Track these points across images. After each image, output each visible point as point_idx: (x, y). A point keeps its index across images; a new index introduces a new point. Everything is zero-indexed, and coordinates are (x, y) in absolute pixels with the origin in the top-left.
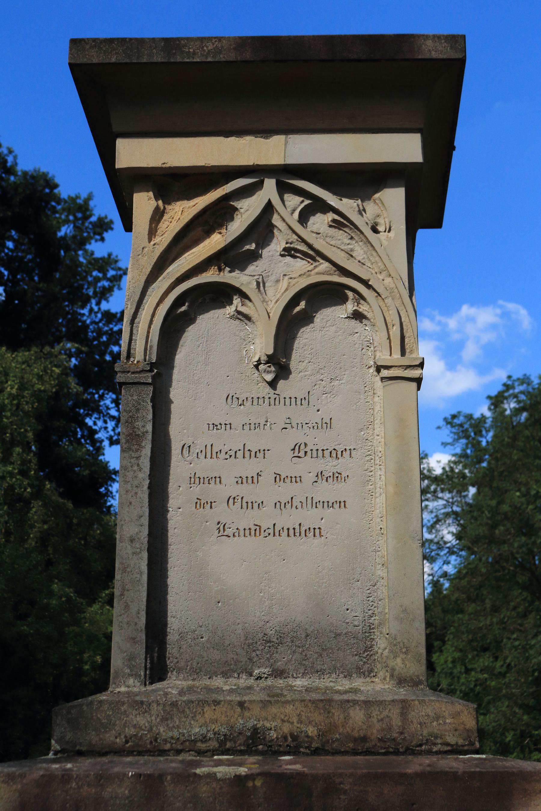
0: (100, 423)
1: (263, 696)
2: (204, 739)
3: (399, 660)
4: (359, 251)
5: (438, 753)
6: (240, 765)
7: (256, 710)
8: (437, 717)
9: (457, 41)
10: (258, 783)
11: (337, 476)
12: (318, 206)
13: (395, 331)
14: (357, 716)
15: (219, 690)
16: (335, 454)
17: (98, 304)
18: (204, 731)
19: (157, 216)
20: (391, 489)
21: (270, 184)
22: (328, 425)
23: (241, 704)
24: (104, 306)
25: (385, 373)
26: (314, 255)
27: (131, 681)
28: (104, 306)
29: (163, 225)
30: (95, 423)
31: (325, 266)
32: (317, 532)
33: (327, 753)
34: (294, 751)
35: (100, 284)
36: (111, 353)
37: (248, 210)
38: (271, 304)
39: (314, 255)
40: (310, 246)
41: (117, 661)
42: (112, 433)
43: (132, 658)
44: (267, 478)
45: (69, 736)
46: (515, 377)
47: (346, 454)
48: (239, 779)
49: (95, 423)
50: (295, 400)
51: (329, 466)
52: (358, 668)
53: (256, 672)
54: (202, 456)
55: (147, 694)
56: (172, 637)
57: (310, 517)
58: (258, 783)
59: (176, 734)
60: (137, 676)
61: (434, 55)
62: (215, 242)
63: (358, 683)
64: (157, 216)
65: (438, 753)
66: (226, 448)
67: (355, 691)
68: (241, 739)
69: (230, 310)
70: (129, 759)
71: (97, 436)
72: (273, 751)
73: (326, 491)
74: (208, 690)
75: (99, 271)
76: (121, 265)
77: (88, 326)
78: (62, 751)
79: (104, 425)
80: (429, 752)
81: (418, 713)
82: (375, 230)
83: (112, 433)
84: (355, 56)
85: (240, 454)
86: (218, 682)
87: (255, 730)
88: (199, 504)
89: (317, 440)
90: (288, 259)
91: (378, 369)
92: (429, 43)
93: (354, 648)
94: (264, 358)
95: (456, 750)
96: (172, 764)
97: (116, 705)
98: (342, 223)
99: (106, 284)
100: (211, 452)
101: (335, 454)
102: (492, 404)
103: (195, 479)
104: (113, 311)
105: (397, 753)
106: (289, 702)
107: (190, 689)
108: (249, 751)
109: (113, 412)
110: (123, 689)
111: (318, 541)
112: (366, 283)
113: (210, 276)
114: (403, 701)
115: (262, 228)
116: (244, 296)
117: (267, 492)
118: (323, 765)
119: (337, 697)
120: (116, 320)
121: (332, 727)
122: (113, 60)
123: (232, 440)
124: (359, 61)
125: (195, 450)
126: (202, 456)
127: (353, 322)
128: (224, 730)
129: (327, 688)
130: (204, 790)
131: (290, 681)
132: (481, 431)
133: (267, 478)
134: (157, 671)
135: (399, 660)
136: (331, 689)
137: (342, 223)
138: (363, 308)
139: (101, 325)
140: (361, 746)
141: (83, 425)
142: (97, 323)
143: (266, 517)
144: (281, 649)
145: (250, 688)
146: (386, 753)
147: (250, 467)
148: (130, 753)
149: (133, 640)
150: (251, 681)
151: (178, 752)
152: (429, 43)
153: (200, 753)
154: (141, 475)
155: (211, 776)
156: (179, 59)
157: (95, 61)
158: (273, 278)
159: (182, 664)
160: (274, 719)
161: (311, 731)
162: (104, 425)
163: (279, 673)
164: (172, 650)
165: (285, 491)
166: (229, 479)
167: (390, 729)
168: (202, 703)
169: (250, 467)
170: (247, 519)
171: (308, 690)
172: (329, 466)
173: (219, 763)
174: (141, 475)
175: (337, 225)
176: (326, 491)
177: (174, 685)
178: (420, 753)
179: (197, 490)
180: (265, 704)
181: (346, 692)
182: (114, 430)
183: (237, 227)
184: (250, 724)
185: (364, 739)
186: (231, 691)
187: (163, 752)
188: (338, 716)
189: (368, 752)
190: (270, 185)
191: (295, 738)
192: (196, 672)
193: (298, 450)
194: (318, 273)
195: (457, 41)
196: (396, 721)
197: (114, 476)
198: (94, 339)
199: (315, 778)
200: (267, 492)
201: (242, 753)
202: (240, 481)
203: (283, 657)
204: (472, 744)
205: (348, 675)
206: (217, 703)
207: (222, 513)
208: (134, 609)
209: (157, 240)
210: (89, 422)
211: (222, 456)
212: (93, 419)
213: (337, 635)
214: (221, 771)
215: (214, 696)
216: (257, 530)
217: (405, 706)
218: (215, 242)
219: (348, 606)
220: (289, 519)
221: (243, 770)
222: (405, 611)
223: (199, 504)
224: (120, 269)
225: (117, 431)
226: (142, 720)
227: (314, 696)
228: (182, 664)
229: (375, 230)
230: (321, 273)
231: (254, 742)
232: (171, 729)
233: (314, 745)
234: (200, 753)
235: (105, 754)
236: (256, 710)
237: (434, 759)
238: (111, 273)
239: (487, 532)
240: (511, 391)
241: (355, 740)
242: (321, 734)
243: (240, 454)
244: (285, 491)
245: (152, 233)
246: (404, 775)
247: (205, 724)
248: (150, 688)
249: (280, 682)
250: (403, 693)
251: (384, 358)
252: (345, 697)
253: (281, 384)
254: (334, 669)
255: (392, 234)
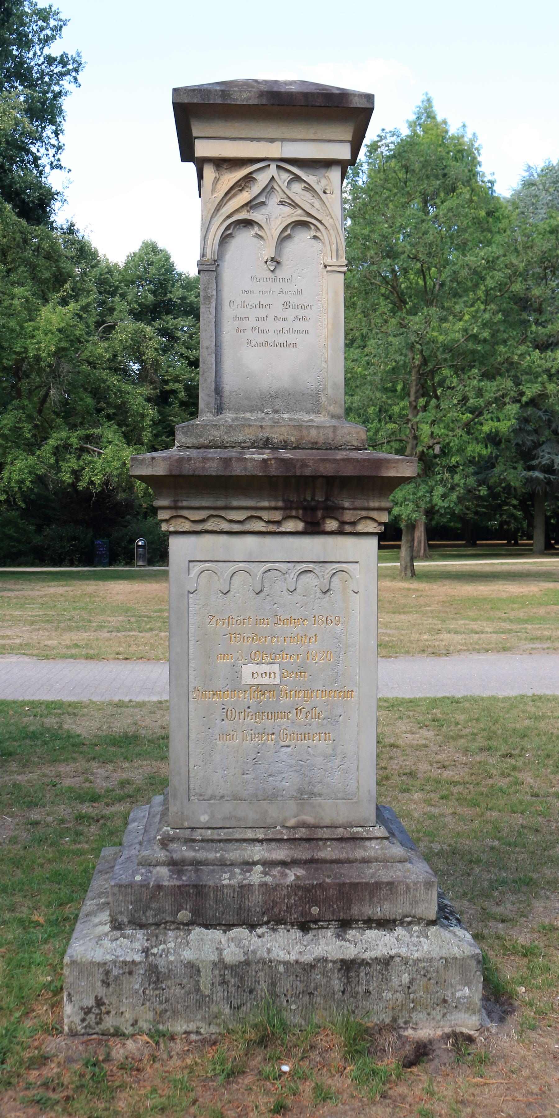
0: (43, 150)
1: (270, 423)
2: (245, 442)
3: (332, 407)
4: (317, 203)
5: (349, 449)
6: (263, 454)
7: (268, 429)
8: (349, 434)
9: (370, 98)
10: (273, 462)
11: (304, 318)
12: (297, 178)
13: (334, 247)
14: (314, 432)
15: (249, 419)
16: (303, 307)
17: (41, 49)
18: (244, 438)
19: (216, 180)
20: (330, 326)
21: (273, 166)
22: (300, 292)
23: (261, 426)
24: (47, 51)
25: (328, 268)
26: (295, 205)
27: (208, 414)
28: (47, 51)
29: (219, 186)
30: (38, 151)
31: (300, 211)
32: (295, 345)
33: (299, 448)
34: (285, 448)
35: (44, 33)
36: (53, 92)
37: (262, 179)
38: (273, 231)
39: (295, 205)
40: (293, 201)
41: (201, 405)
42: (52, 159)
43: (208, 404)
44: (271, 318)
45: (183, 440)
46: (387, 130)
47: (309, 308)
48: (264, 461)
49: (38, 151)
50: (284, 280)
51: (301, 313)
52: (313, 410)
53: (265, 411)
54: (239, 307)
55: (218, 421)
56: (226, 394)
57: (291, 338)
58: (273, 462)
59: (232, 439)
60: (211, 412)
61: (359, 106)
62: (245, 197)
63: (313, 417)
64: (216, 180)
65: (349, 449)
66: (250, 303)
67: (312, 421)
68: (261, 442)
69: (253, 233)
70: (212, 450)
71: (39, 162)
72: (276, 448)
73: (299, 325)
74: (246, 419)
75: (44, 22)
76: (61, 16)
77: (32, 68)
78: (180, 446)
79: (46, 152)
80: (345, 449)
81: (340, 432)
82: (325, 192)
83: (52, 159)
84: (318, 104)
85: (258, 306)
86: (248, 415)
87: (268, 439)
88: (238, 330)
89: (295, 300)
90: (281, 206)
91: (325, 266)
92: (356, 98)
93: (312, 401)
94: (269, 259)
95: (357, 449)
96: (233, 453)
97: (204, 426)
98: (309, 188)
99: (49, 32)
100: (244, 305)
101: (303, 307)
102: (368, 151)
103: (236, 318)
104: (53, 55)
105: (331, 449)
106: (283, 424)
107: (236, 418)
108: (265, 447)
109: (54, 141)
110: (205, 418)
111: (295, 349)
112: (320, 221)
113: (243, 215)
114: (334, 426)
115: (269, 189)
116: (260, 226)
117: (271, 325)
118: (299, 455)
119: (304, 424)
120: (56, 63)
121: (302, 438)
122: (195, 101)
123: (254, 299)
124: (320, 106)
125: (236, 304)
126: (239, 307)
127: (313, 241)
128: (254, 438)
129: (299, 419)
130: (249, 465)
131: (281, 415)
132: (358, 173)
133: (271, 318)
134: (219, 410)
135: (332, 407)
136: (301, 419)
137: (309, 188)
138: (318, 234)
139: (43, 67)
140: (315, 446)
141: (28, 152)
142: (39, 65)
143: (271, 338)
144: (277, 400)
145: (263, 418)
146: (326, 449)
147: (262, 313)
148: (211, 448)
149: (209, 395)
150: (263, 415)
151: (233, 447)
152: (356, 98)
153: (243, 448)
154: (211, 317)
155: (252, 459)
156: (229, 102)
157: (186, 101)
158: (274, 216)
159: (231, 406)
160: (276, 433)
161: (293, 439)
162: (46, 152)
163: (276, 412)
164: (225, 400)
165: (279, 325)
166: (252, 319)
167: (328, 439)
168: (243, 426)
169: (262, 313)
170: (261, 338)
171: (290, 420)
172: (301, 313)
173: (253, 453)
174: (211, 317)
175: (306, 189)
176: (299, 325)
177: (228, 416)
178: (341, 449)
179: (237, 323)
180: (272, 427)
181: (308, 421)
182: (54, 156)
183: (256, 189)
184: (266, 435)
185: (316, 443)
186: (255, 420)
187: (226, 448)
188: (305, 432)
189: (318, 449)
190: (273, 166)
191: (285, 442)
192: (237, 410)
193: (286, 305)
194: (297, 215)
195: (370, 98)
196: (331, 435)
197: (56, 196)
198: (38, 79)
199: (297, 460)
200: (271, 325)
201: (262, 448)
202: (258, 319)
203: (278, 404)
204: (364, 446)
205: (308, 413)
206: (250, 426)
207: (249, 334)
208: (209, 381)
209: (216, 195)
210: (34, 149)
211: (249, 307)
212: (37, 146)
213: (303, 394)
214: (256, 456)
215: (249, 423)
216: (266, 344)
217: (335, 428)
218: (245, 197)
219: (309, 381)
220: (281, 339)
221: (265, 457)
222: (335, 384)
223: (238, 330)
224: (61, 20)
225: (56, 158)
226: (216, 433)
227: (294, 423)
228: (231, 406)
229: (325, 192)
230: (297, 215)
231: (267, 444)
232: (230, 437)
233: (294, 445)
234: (243, 448)
235: (200, 448)
236: (268, 429)
237: (348, 452)
238: (52, 23)
239: (360, 255)
240: (384, 142)
241: (312, 443)
242: (297, 440)
243: (258, 306)
244: (279, 325)
245: (213, 190)
246: (335, 460)
247: (245, 435)
248: (218, 417)
249: (277, 416)
250: (334, 422)
251: (329, 261)
252: (308, 424)
253: (277, 272)
254: (302, 410)
255: (333, 196)
